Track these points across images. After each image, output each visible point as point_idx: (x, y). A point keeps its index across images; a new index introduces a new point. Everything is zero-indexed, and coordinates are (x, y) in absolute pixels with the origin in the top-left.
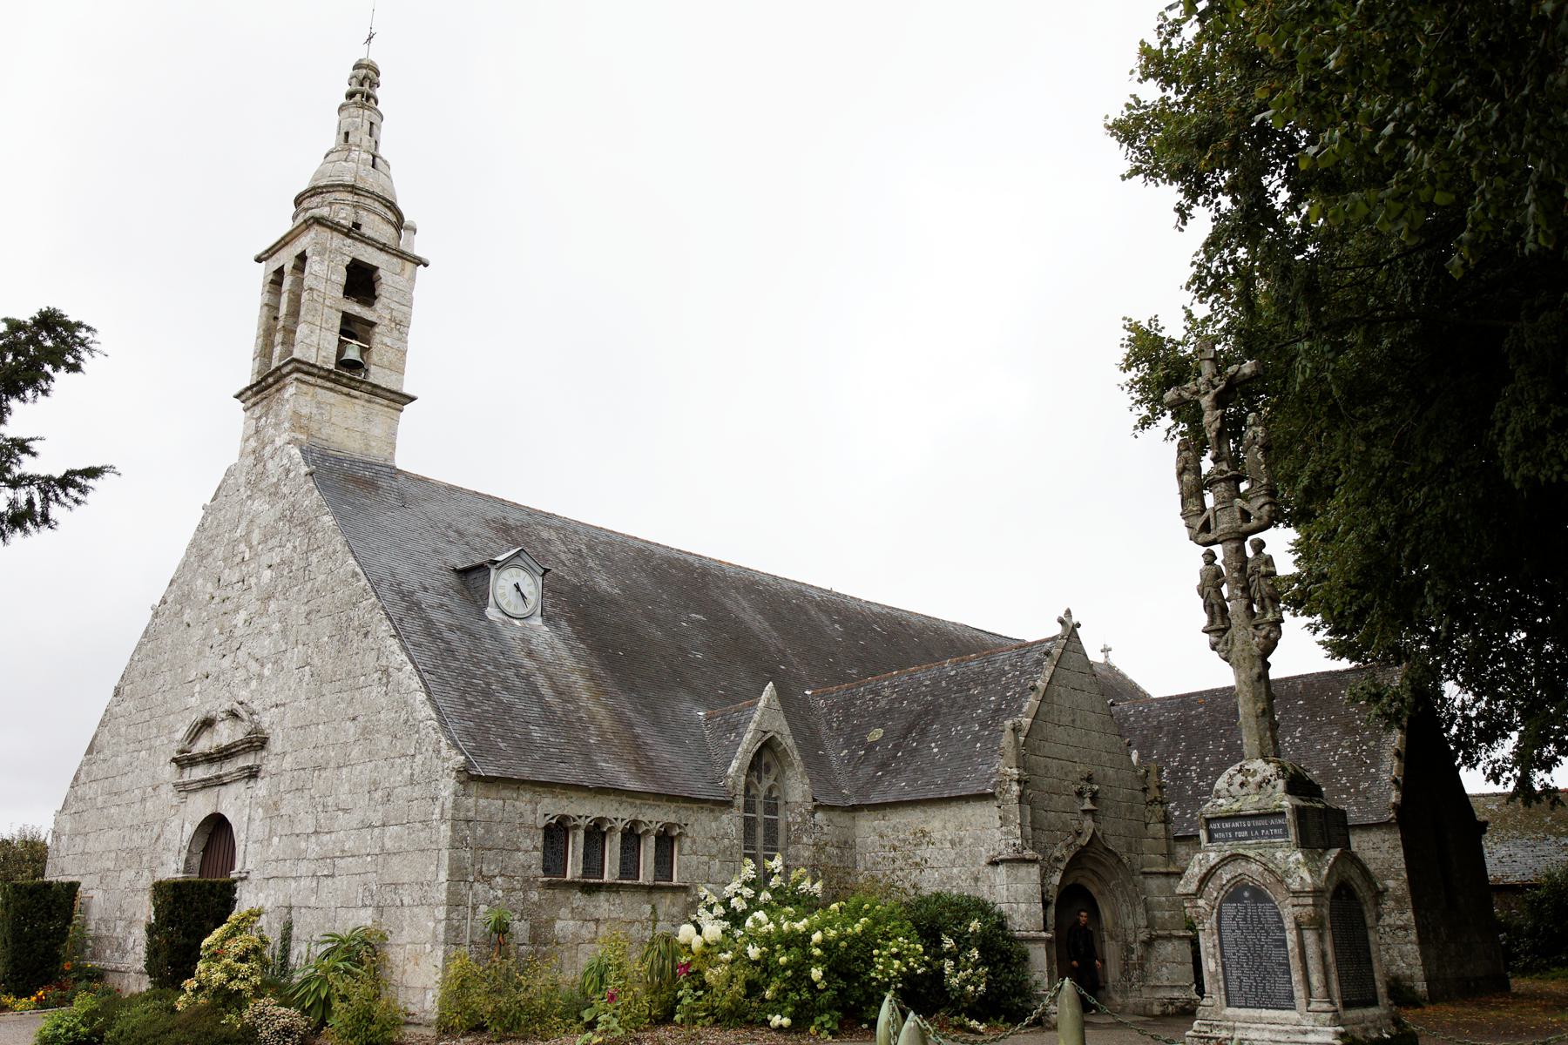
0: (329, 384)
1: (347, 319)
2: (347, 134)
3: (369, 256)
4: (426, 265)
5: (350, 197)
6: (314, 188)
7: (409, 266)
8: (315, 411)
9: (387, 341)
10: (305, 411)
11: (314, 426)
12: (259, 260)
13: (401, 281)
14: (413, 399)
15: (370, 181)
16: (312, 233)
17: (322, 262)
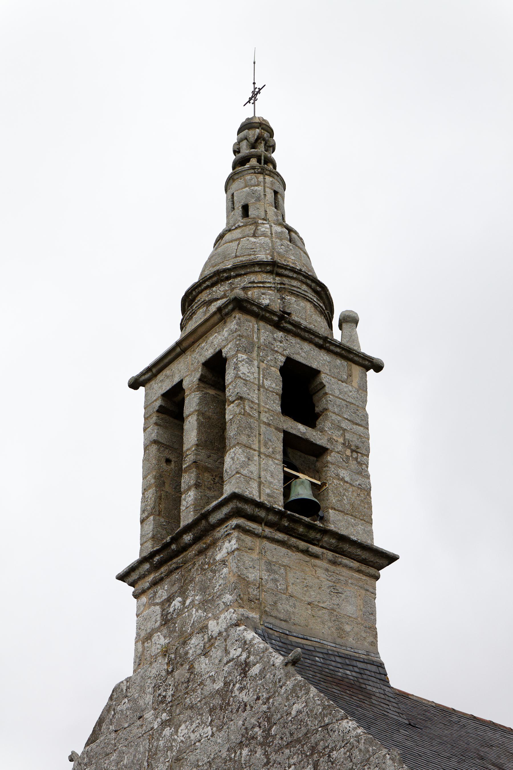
0: (280, 536)
1: (290, 441)
2: (245, 209)
3: (308, 355)
4: (378, 367)
5: (269, 278)
6: (217, 273)
7: (356, 370)
8: (265, 576)
9: (343, 473)
10: (252, 576)
11: (267, 598)
12: (135, 384)
13: (349, 390)
14: (390, 558)
15: (291, 259)
16: (232, 325)
17: (250, 362)
